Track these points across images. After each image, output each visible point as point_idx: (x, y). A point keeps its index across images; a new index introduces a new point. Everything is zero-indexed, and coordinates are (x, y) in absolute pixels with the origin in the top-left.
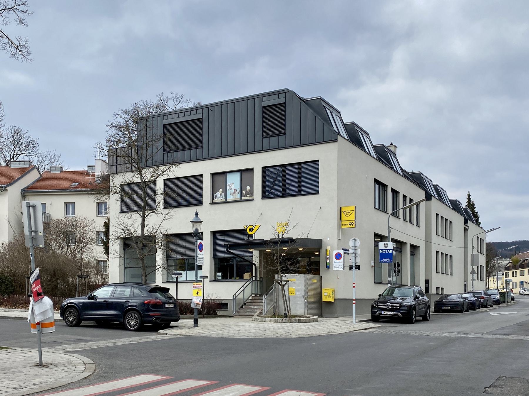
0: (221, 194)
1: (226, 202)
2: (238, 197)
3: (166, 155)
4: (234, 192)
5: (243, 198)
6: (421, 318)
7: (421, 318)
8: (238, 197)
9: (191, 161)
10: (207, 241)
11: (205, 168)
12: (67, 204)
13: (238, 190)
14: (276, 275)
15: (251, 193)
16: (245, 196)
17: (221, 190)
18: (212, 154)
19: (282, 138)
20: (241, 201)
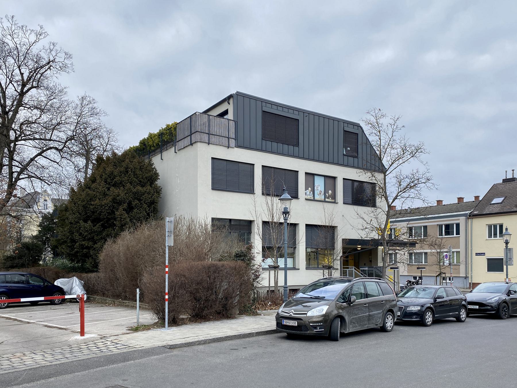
0: (310, 192)
1: (314, 200)
2: (322, 198)
3: (264, 142)
4: (320, 193)
5: (327, 200)
6: (455, 319)
7: (455, 319)
8: (322, 198)
9: (283, 154)
10: (302, 232)
11: (302, 166)
12: (490, 227)
13: (323, 192)
14: (55, 221)
15: (334, 196)
16: (331, 198)
17: (310, 189)
18: (311, 157)
19: (296, 148)
20: (325, 201)
